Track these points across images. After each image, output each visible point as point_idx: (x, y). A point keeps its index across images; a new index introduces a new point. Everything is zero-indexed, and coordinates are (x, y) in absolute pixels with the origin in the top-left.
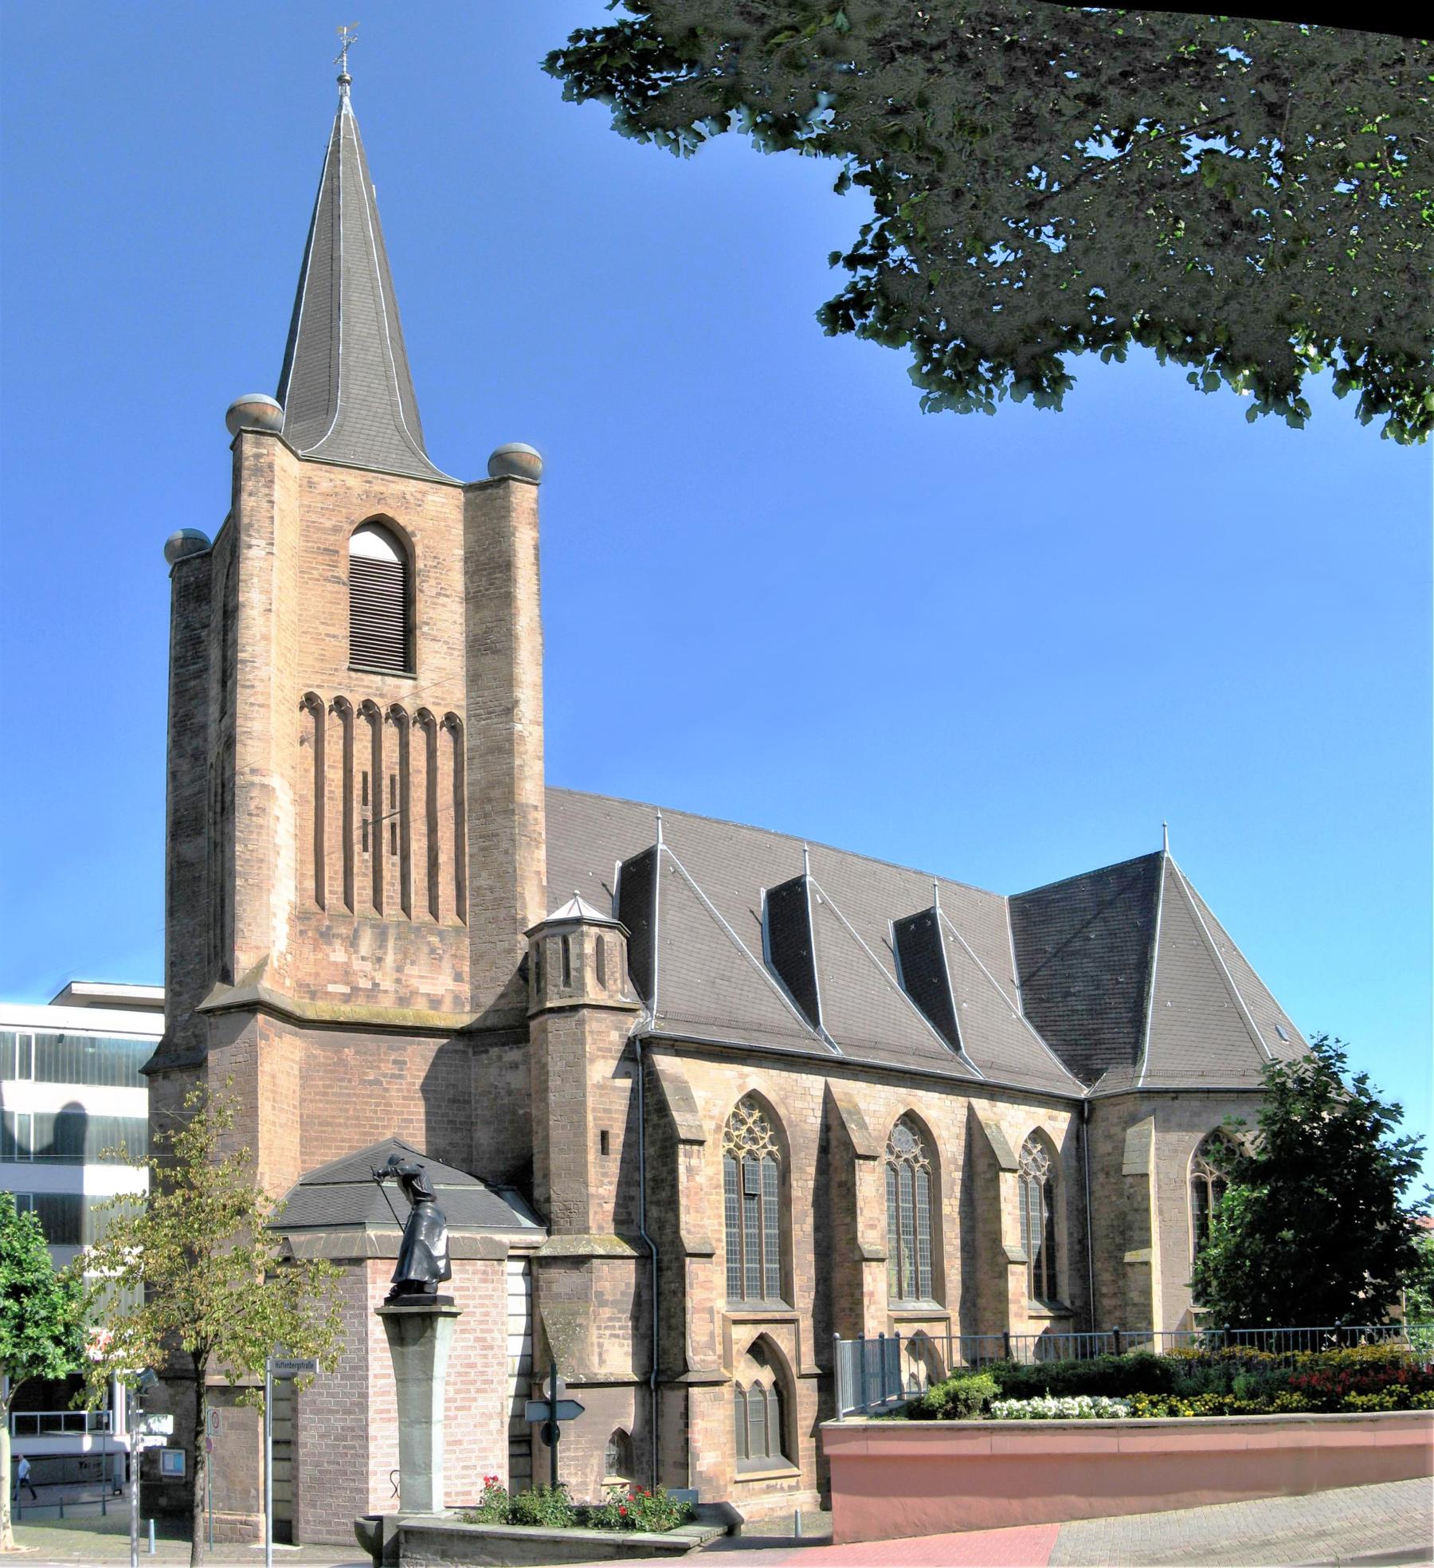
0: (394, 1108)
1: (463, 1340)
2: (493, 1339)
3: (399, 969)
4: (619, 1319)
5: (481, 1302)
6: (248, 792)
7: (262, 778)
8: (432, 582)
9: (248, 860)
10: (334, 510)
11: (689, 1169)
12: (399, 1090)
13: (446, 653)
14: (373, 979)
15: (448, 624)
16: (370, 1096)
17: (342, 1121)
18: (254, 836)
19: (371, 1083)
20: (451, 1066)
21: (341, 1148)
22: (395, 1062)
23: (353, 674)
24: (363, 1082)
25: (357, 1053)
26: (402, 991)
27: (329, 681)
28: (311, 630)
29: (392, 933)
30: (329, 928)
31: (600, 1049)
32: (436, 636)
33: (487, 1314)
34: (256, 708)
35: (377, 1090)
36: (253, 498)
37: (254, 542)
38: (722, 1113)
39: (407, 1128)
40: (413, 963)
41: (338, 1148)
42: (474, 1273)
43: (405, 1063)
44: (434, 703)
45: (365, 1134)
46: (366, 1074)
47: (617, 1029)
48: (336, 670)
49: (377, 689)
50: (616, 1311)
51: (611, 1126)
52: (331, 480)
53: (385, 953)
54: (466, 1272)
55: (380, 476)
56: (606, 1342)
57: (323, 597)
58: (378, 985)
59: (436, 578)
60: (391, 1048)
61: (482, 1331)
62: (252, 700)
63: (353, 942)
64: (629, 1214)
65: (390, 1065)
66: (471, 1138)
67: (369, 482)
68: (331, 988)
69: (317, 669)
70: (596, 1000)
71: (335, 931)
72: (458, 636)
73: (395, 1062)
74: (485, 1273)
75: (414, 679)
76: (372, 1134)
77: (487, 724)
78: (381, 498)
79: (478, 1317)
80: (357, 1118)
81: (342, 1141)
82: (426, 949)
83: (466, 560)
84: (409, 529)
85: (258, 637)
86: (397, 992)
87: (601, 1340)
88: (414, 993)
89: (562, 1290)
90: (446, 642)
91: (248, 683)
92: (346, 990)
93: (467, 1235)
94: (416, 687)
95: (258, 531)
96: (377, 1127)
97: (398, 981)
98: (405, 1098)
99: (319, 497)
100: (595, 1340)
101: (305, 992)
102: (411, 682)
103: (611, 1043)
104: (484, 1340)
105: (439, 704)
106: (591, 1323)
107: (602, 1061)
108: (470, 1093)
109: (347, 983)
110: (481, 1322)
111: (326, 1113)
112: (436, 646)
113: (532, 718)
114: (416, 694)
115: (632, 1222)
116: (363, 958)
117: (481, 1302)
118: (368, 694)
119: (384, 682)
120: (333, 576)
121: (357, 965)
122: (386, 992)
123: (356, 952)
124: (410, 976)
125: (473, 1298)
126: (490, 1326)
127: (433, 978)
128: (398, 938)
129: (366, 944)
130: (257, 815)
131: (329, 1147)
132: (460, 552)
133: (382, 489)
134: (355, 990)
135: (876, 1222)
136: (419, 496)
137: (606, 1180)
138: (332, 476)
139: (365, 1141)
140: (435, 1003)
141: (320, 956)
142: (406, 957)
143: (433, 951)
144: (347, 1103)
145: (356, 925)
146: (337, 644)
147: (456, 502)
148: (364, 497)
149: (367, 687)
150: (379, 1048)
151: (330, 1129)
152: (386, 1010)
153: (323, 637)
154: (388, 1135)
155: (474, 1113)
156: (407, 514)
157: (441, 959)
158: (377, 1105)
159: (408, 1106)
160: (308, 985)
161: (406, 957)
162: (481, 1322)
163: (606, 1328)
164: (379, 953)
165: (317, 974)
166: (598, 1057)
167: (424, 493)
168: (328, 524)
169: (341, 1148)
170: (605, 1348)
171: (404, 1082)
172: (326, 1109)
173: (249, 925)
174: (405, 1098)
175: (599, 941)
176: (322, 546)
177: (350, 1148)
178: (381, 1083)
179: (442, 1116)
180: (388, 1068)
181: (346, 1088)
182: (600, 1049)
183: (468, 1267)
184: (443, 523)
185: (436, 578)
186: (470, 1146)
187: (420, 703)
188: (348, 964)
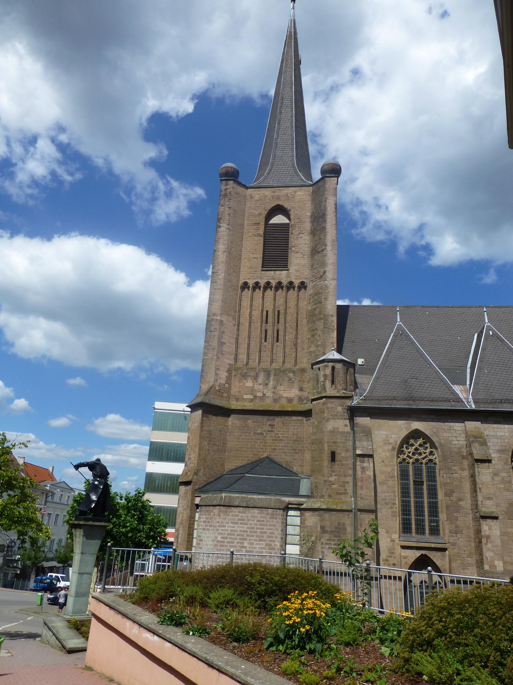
1: (260, 544)
2: (275, 545)
3: (275, 388)
5: (270, 527)
6: (211, 323)
7: (216, 317)
8: (297, 229)
9: (208, 349)
10: (259, 207)
11: (363, 468)
12: (271, 437)
14: (263, 392)
15: (303, 245)
16: (257, 439)
17: (245, 449)
18: (212, 339)
19: (258, 434)
20: (295, 426)
21: (244, 460)
22: (270, 425)
23: (263, 272)
25: (253, 422)
26: (276, 396)
28: (247, 257)
29: (272, 373)
30: (246, 373)
31: (331, 415)
32: (298, 251)
33: (272, 533)
34: (217, 290)
35: (261, 437)
37: (222, 225)
38: (396, 442)
39: (273, 452)
40: (281, 385)
41: (242, 460)
42: (267, 514)
43: (274, 425)
44: (295, 279)
45: (254, 455)
47: (341, 406)
48: (256, 271)
49: (272, 276)
50: (332, 536)
51: (337, 449)
52: (259, 194)
53: (269, 382)
55: (278, 189)
56: (326, 551)
59: (298, 227)
60: (268, 420)
61: (269, 541)
62: (216, 287)
63: (256, 378)
64: (346, 490)
66: (303, 457)
68: (245, 397)
69: (249, 272)
70: (330, 394)
71: (248, 374)
73: (270, 425)
74: (273, 514)
75: (288, 270)
76: (258, 455)
77: (315, 283)
78: (278, 198)
79: (268, 534)
81: (245, 457)
82: (287, 379)
84: (289, 208)
85: (220, 263)
86: (273, 397)
88: (281, 397)
89: (309, 524)
90: (302, 253)
91: (214, 281)
92: (252, 397)
93: (269, 497)
97: (274, 393)
98: (273, 440)
99: (254, 203)
101: (234, 399)
102: (286, 272)
103: (337, 412)
104: (270, 545)
105: (298, 279)
106: (318, 541)
107: (332, 420)
109: (252, 394)
110: (269, 537)
111: (238, 446)
112: (297, 255)
113: (332, 277)
114: (288, 277)
115: (348, 493)
116: (259, 384)
117: (270, 527)
118: (268, 279)
119: (275, 273)
120: (258, 234)
121: (257, 387)
122: (268, 397)
123: (257, 382)
124: (280, 390)
125: (266, 525)
126: (274, 539)
128: (275, 375)
129: (261, 378)
130: (214, 332)
131: (239, 460)
133: (279, 194)
134: (255, 397)
136: (293, 193)
137: (333, 474)
139: (254, 458)
140: (290, 400)
141: (242, 384)
145: (257, 371)
147: (308, 193)
148: (271, 199)
149: (268, 276)
152: (268, 404)
153: (252, 259)
154: (265, 455)
157: (293, 382)
159: (275, 443)
160: (236, 396)
162: (269, 537)
163: (326, 544)
164: (267, 382)
165: (240, 391)
166: (331, 419)
167: (295, 192)
168: (257, 213)
169: (244, 460)
170: (325, 554)
171: (273, 433)
174: (273, 440)
175: (333, 368)
177: (248, 460)
178: (263, 434)
179: (290, 447)
180: (267, 428)
181: (248, 436)
182: (331, 415)
183: (264, 512)
185: (298, 227)
187: (289, 280)
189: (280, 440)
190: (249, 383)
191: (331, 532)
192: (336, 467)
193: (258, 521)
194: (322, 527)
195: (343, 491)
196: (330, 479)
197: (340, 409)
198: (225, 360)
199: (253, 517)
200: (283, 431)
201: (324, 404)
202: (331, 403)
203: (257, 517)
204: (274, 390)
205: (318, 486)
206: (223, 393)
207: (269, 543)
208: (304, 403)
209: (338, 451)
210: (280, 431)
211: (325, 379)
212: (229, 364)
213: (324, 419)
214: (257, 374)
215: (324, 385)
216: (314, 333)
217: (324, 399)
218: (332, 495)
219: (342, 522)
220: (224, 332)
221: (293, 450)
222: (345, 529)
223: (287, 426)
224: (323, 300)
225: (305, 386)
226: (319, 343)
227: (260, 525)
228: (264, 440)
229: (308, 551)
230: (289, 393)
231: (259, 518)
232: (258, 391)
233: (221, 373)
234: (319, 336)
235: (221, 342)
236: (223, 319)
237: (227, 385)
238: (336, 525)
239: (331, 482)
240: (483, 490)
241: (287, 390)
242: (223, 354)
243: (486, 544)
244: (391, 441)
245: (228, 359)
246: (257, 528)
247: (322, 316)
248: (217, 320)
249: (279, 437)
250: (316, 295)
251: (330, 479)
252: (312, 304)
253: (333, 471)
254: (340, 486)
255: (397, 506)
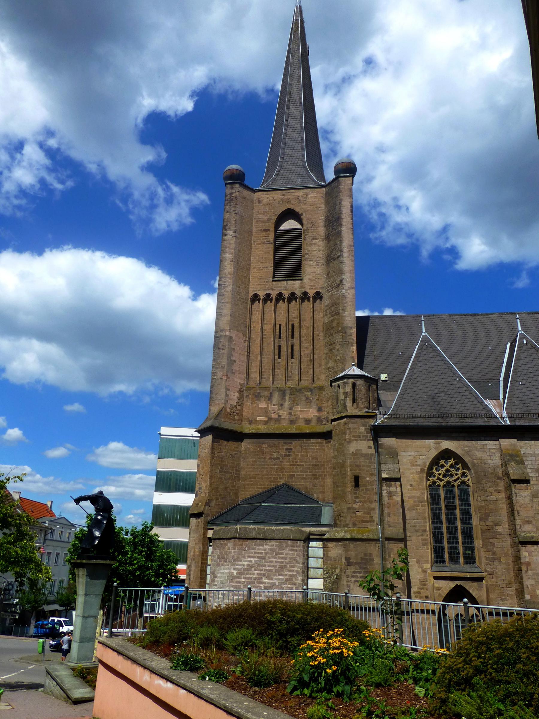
0: (286, 470)
1: (280, 579)
4: (360, 573)
5: (290, 560)
8: (310, 234)
9: (217, 368)
11: (390, 493)
13: (316, 265)
14: (278, 414)
16: (274, 465)
17: (260, 476)
19: (275, 459)
21: (260, 488)
22: (287, 449)
23: (274, 283)
24: (271, 459)
25: (269, 446)
26: (292, 418)
27: (263, 288)
29: (288, 392)
30: (259, 393)
31: (354, 436)
32: (311, 258)
33: (293, 567)
35: (277, 462)
36: (228, 213)
37: (228, 232)
38: (425, 463)
39: (292, 478)
40: (298, 405)
41: (258, 488)
42: (286, 546)
43: (291, 449)
45: (271, 482)
46: (272, 455)
47: (363, 425)
48: (267, 282)
51: (360, 474)
53: (285, 402)
54: (282, 546)
55: (288, 191)
56: (352, 585)
57: (262, 251)
58: (281, 416)
60: (285, 443)
61: (290, 575)
63: (270, 398)
64: (372, 517)
65: (284, 451)
67: (283, 195)
68: (259, 419)
71: (262, 394)
72: (321, 256)
73: (287, 449)
75: (301, 280)
76: (274, 482)
78: (289, 201)
80: (268, 475)
81: (260, 485)
82: (304, 398)
83: (325, 221)
84: (300, 212)
87: (349, 583)
88: (298, 418)
90: (316, 260)
92: (266, 419)
93: (288, 528)
94: (301, 283)
95: (230, 228)
96: (277, 478)
97: (290, 413)
98: (291, 465)
99: (262, 207)
100: (345, 583)
102: (300, 281)
104: (291, 580)
105: (312, 289)
106: (343, 574)
108: (324, 462)
109: (266, 416)
110: (289, 571)
114: (302, 286)
116: (274, 405)
117: (290, 560)
118: (280, 290)
119: (287, 284)
121: (271, 408)
122: (284, 419)
123: (271, 402)
125: (286, 558)
126: (294, 573)
127: (307, 411)
128: (291, 394)
129: (276, 398)
130: (223, 349)
131: (254, 488)
132: (323, 218)
133: (289, 197)
134: (270, 419)
135: (531, 519)
136: (305, 196)
137: (357, 500)
138: (268, 196)
140: (308, 422)
142: (294, 403)
143: (307, 399)
144: (263, 468)
145: (271, 391)
146: (267, 270)
147: (321, 195)
150: (279, 443)
151: (254, 480)
152: (284, 427)
155: (325, 470)
156: (300, 206)
157: (311, 402)
158: (278, 468)
159: (293, 469)
160: (248, 418)
161: (294, 403)
162: (289, 571)
163: (352, 577)
164: (282, 402)
165: (253, 413)
166: (353, 440)
167: (307, 194)
168: (266, 218)
169: (260, 488)
170: (351, 588)
171: (291, 458)
172: (253, 471)
173: (216, 395)
174: (291, 465)
175: (354, 385)
176: (263, 229)
177: (264, 488)
179: (310, 472)
180: (284, 452)
181: (263, 462)
182: (354, 436)
183: (283, 544)
184: (315, 206)
186: (324, 486)
187: (303, 290)
188: (267, 408)
189: (298, 465)
190: (263, 404)
191: (357, 564)
192: (360, 493)
193: (277, 554)
194: (347, 559)
195: (368, 519)
196: (354, 506)
197: (362, 429)
198: (236, 380)
199: (271, 549)
200: (302, 455)
201: (345, 424)
202: (353, 423)
203: (275, 550)
204: (290, 411)
205: (342, 514)
206: (234, 415)
207: (289, 577)
208: (323, 423)
209: (362, 476)
210: (298, 455)
211: (346, 398)
212: (240, 384)
213: (345, 440)
214: (271, 393)
215: (345, 404)
216: (331, 347)
217: (345, 419)
218: (357, 523)
219: (369, 552)
220: (234, 349)
221: (313, 475)
222: (372, 560)
223: (305, 449)
224: (341, 311)
225: (324, 405)
226: (337, 358)
227: (279, 558)
228: (281, 465)
229: (333, 585)
230: (307, 413)
231: (278, 551)
232: (273, 412)
233: (232, 393)
234: (338, 350)
235: (231, 360)
236: (232, 335)
237: (238, 407)
238: (362, 555)
239: (356, 509)
240: (521, 513)
241: (304, 411)
242: (233, 373)
243: (526, 572)
244: (420, 462)
245: (239, 378)
246: (276, 562)
247: (340, 329)
248: (226, 336)
249: (297, 462)
250: (333, 306)
251: (354, 506)
252: (329, 316)
253: (357, 497)
254: (365, 513)
255: (428, 533)
